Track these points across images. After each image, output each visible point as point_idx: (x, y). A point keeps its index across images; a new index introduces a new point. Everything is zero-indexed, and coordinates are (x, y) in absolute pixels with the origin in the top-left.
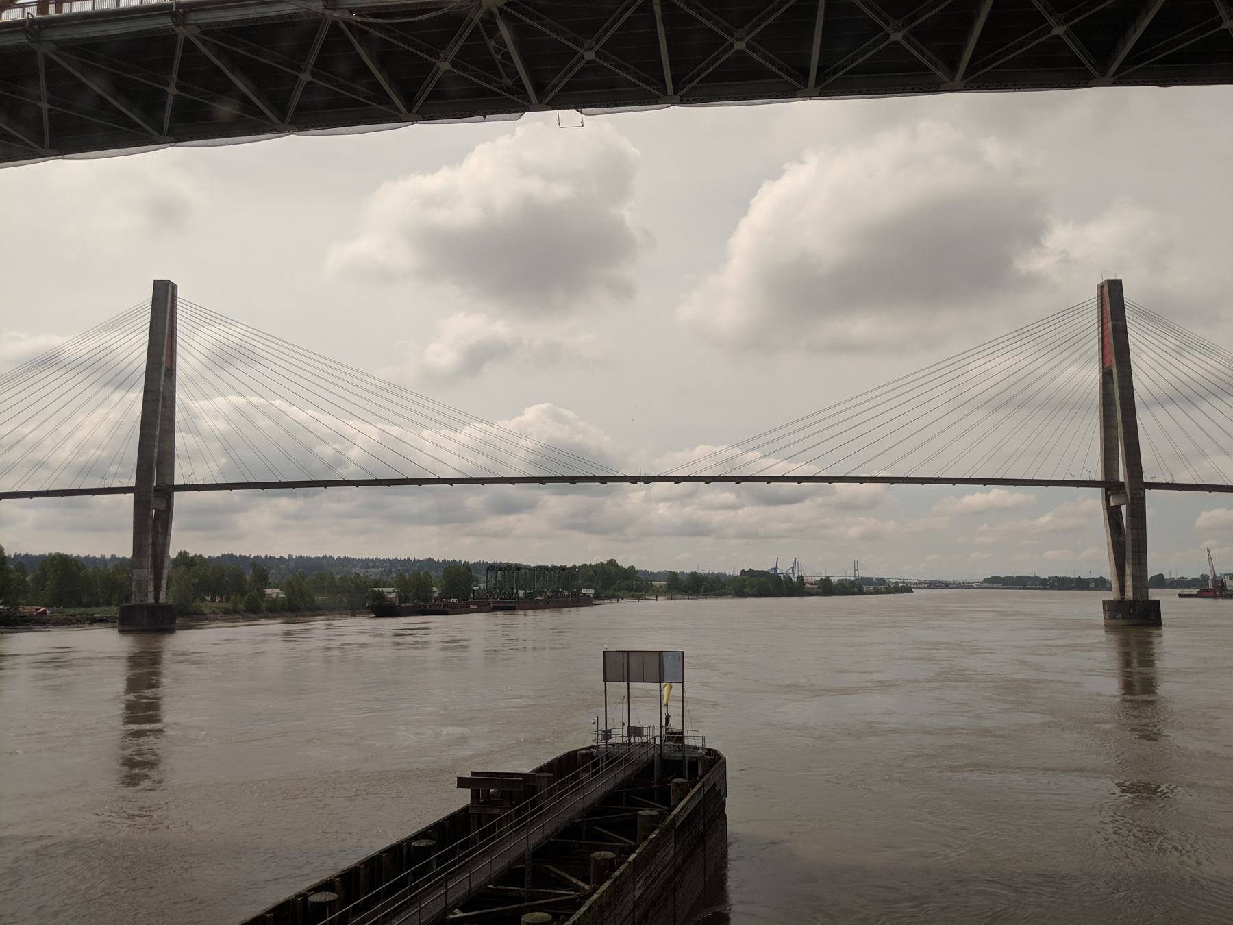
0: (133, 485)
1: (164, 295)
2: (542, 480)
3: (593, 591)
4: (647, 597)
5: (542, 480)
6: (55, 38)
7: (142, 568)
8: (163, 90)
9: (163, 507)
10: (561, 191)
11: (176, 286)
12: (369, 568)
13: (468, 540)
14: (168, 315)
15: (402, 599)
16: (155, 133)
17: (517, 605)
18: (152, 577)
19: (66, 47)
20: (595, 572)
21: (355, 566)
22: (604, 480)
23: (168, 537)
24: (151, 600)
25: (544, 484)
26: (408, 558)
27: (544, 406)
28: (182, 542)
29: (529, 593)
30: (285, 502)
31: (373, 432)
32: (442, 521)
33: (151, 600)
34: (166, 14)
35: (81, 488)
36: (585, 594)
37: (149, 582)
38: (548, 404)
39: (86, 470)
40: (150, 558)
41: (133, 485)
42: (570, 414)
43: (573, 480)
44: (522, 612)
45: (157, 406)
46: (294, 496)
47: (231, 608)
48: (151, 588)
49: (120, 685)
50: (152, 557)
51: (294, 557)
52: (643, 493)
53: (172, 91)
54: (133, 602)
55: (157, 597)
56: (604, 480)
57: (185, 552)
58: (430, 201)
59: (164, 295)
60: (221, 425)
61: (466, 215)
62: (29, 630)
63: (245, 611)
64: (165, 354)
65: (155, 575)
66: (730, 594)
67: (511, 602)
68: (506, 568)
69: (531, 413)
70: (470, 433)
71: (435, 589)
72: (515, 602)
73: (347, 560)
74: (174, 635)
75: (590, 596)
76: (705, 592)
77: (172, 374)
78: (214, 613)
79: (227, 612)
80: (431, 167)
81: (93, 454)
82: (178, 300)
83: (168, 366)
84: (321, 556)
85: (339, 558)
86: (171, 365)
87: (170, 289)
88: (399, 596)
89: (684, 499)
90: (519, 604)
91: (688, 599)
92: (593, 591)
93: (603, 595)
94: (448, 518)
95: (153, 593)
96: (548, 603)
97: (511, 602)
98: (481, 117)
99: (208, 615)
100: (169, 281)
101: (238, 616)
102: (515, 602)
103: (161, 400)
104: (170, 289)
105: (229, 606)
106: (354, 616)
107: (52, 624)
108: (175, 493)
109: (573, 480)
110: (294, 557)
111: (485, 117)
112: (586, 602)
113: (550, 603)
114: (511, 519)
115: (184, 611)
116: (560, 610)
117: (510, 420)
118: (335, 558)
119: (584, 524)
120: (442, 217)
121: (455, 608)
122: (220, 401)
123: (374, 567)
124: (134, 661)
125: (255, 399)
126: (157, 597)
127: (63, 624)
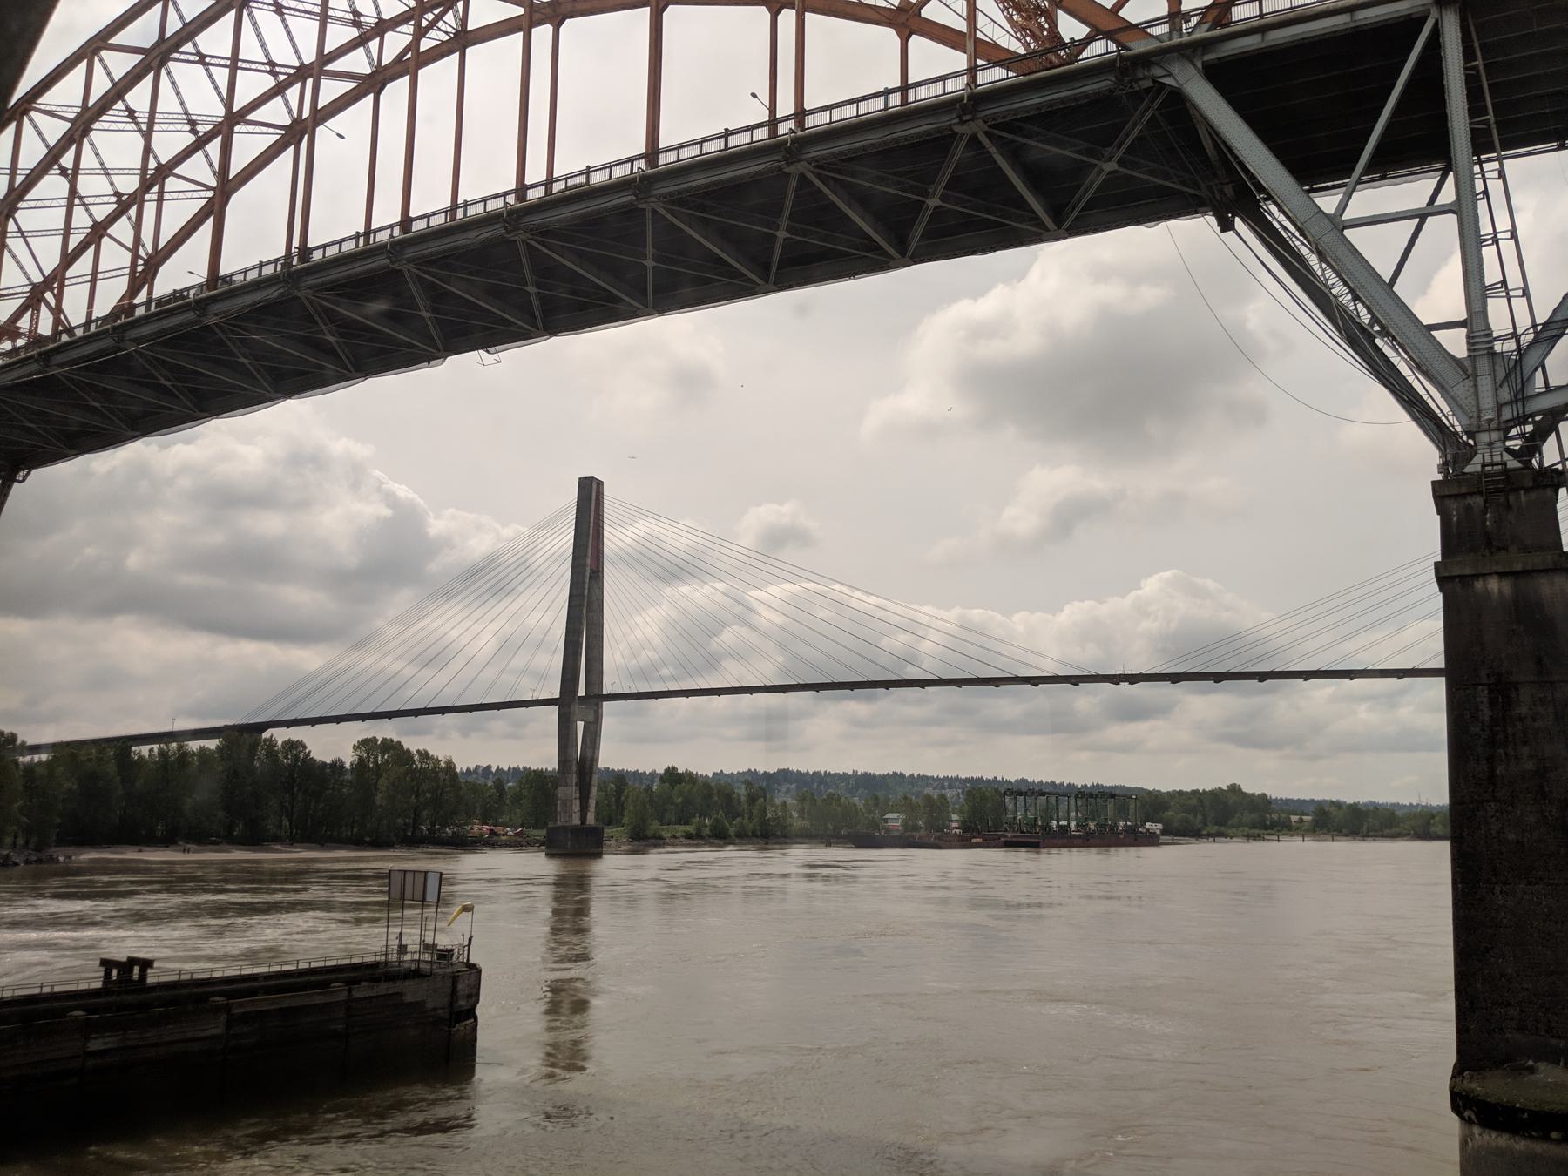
0: (557, 695)
1: (590, 494)
2: (1175, 678)
3: (1160, 826)
4: (1266, 837)
5: (1175, 678)
6: (133, 337)
7: (566, 786)
8: (773, 234)
9: (591, 718)
10: (1151, 296)
11: (602, 482)
12: (944, 788)
13: (1085, 755)
14: (593, 514)
15: (909, 826)
16: (641, 306)
17: (1041, 841)
18: (578, 796)
19: (678, 201)
20: (1200, 801)
21: (928, 786)
22: (1262, 676)
23: (596, 751)
24: (576, 821)
25: (998, 686)
26: (996, 778)
27: (1168, 574)
28: (614, 755)
29: (1062, 826)
30: (857, 706)
31: (954, 614)
32: (1056, 728)
33: (576, 821)
34: (189, 310)
35: (512, 700)
36: (1148, 830)
37: (574, 801)
38: (1174, 571)
39: (644, 674)
40: (574, 775)
41: (557, 695)
42: (1211, 585)
43: (1218, 677)
44: (1045, 850)
45: (582, 610)
46: (869, 699)
47: (694, 832)
48: (576, 807)
49: (548, 913)
50: (577, 774)
51: (859, 773)
52: (1333, 688)
53: (782, 234)
54: (559, 823)
55: (583, 818)
56: (1262, 676)
57: (674, 768)
58: (979, 332)
59: (590, 494)
60: (779, 619)
61: (1025, 342)
62: (473, 851)
63: (709, 836)
64: (589, 554)
65: (580, 794)
66: (1407, 835)
67: (1034, 837)
68: (1097, 795)
69: (1151, 586)
70: (1072, 614)
71: (955, 817)
72: (1038, 837)
73: (922, 778)
74: (599, 860)
75: (1155, 833)
76: (1368, 831)
77: (599, 576)
78: (674, 837)
79: (689, 836)
80: (978, 293)
81: (648, 656)
82: (605, 497)
83: (595, 568)
84: (891, 773)
85: (912, 775)
86: (598, 567)
87: (594, 486)
88: (905, 825)
89: (1391, 700)
90: (1044, 840)
91: (1333, 841)
92: (1160, 826)
93: (1205, 832)
94: (1063, 726)
95: (579, 814)
96: (1088, 840)
97: (1034, 837)
98: (426, 364)
99: (667, 840)
100: (593, 478)
101: (700, 841)
102: (1038, 837)
103: (585, 603)
104: (594, 486)
105: (690, 829)
106: (829, 845)
107: (500, 846)
108: (604, 703)
109: (1218, 677)
110: (859, 773)
111: (429, 363)
112: (1151, 840)
113: (1091, 840)
114: (1140, 728)
115: (641, 835)
116: (1107, 849)
117: (1123, 596)
118: (711, 776)
119: (1248, 737)
120: (993, 350)
121: (950, 841)
122: (773, 589)
123: (950, 787)
124: (561, 882)
125: (811, 586)
126: (583, 818)
127: (511, 846)
